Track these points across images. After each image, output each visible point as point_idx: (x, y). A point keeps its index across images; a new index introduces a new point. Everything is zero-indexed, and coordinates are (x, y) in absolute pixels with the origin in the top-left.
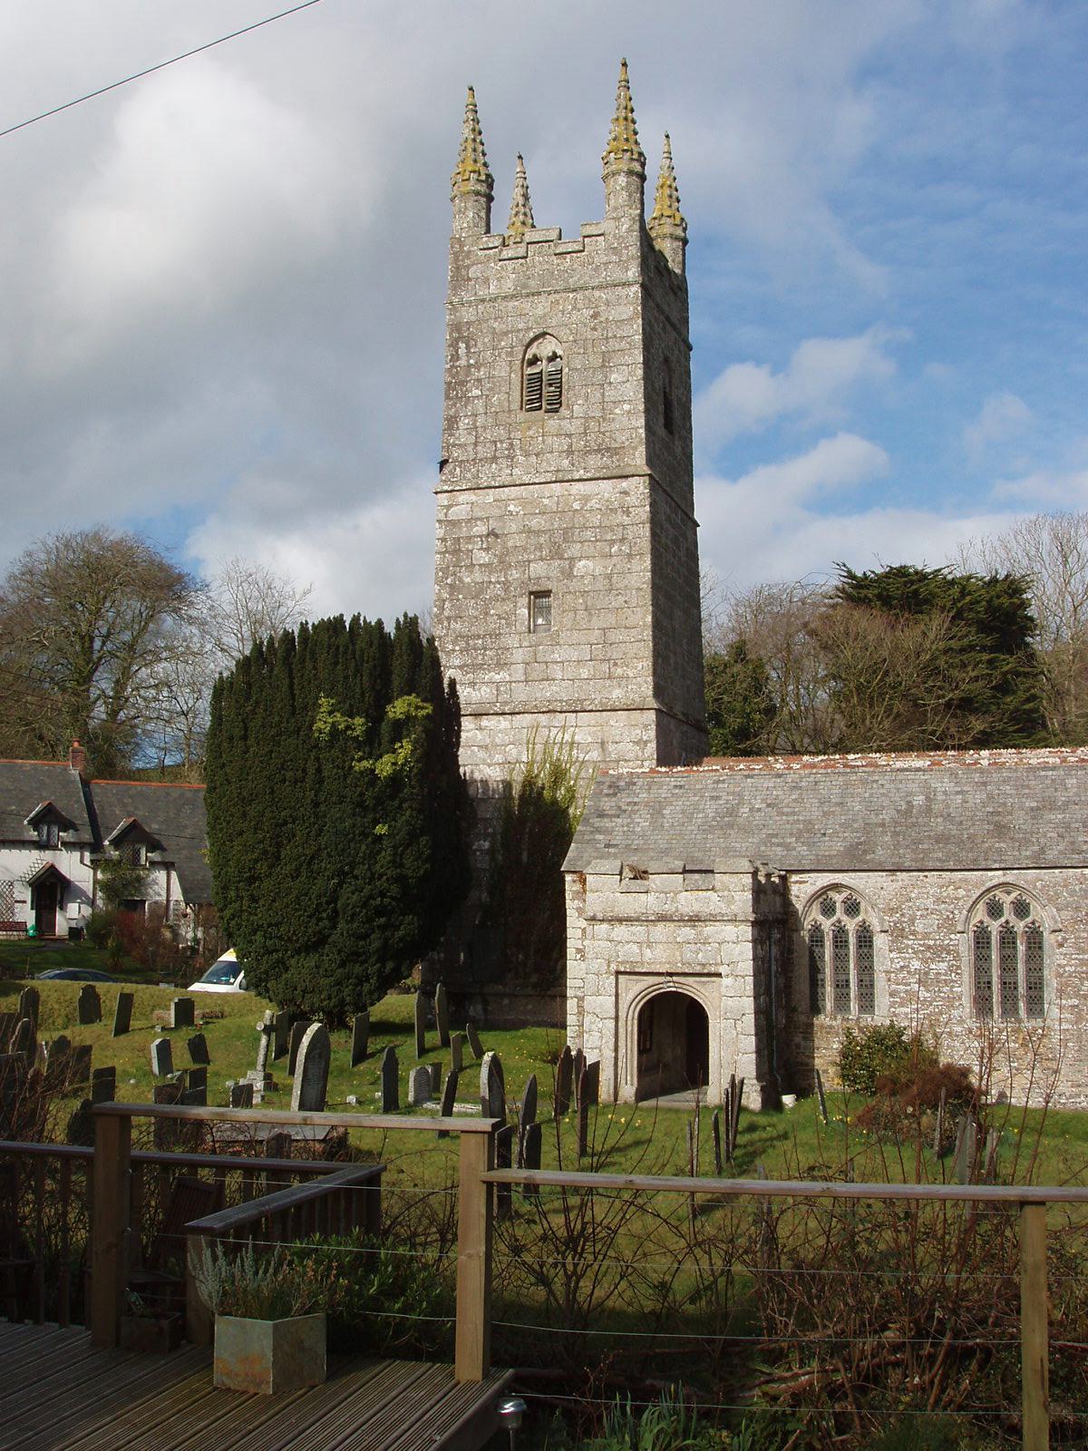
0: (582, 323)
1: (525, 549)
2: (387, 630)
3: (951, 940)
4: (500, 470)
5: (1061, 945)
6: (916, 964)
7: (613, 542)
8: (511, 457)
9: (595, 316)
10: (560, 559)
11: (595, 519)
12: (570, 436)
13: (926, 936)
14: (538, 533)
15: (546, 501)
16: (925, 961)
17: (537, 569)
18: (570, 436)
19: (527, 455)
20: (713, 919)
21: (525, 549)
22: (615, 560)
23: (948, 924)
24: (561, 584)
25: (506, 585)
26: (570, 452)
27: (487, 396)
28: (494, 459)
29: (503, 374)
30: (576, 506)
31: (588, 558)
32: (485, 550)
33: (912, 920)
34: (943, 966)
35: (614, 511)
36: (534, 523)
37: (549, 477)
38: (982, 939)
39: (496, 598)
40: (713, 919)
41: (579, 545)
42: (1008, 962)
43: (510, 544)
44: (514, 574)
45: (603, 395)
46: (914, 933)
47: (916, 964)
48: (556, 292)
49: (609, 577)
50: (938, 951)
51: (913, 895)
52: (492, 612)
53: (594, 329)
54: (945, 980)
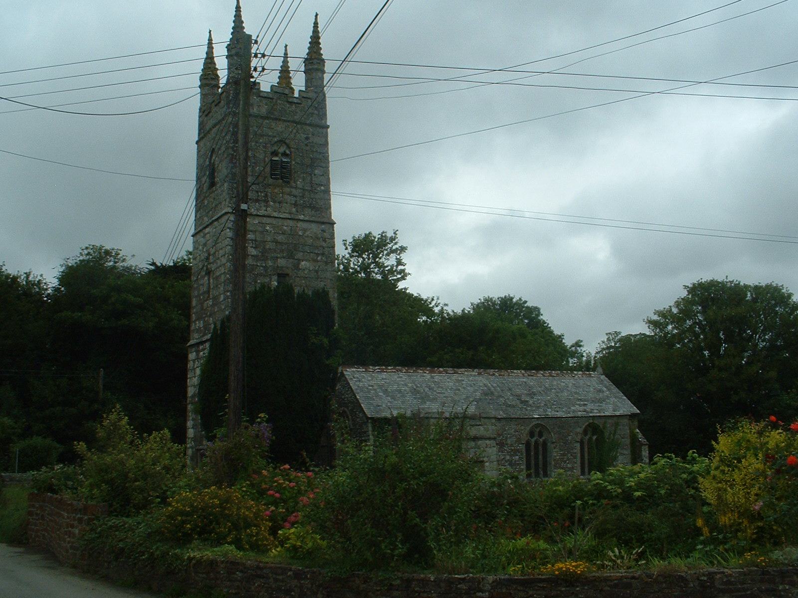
0: (301, 140)
1: (275, 251)
2: (648, 334)
3: (520, 447)
4: (261, 207)
5: (555, 448)
6: (508, 457)
7: (318, 255)
8: (266, 202)
9: (307, 138)
10: (293, 259)
11: (310, 241)
12: (295, 196)
13: (511, 445)
14: (281, 243)
15: (285, 228)
16: (511, 456)
17: (281, 262)
18: (295, 196)
19: (274, 202)
20: (482, 438)
21: (275, 251)
22: (319, 263)
23: (519, 441)
24: (293, 272)
25: (266, 268)
26: (295, 205)
27: (253, 166)
28: (257, 201)
29: (261, 157)
30: (300, 233)
31: (306, 260)
32: (254, 248)
33: (507, 438)
34: (517, 457)
35: (318, 238)
36: (280, 238)
37: (287, 216)
38: (528, 444)
39: (261, 275)
40: (482, 438)
41: (302, 254)
42: (537, 454)
43: (267, 247)
44: (270, 263)
45: (311, 179)
46: (507, 444)
47: (508, 457)
48: (289, 121)
49: (317, 272)
50: (516, 452)
51: (507, 429)
52: (259, 281)
53: (306, 145)
54: (518, 463)
